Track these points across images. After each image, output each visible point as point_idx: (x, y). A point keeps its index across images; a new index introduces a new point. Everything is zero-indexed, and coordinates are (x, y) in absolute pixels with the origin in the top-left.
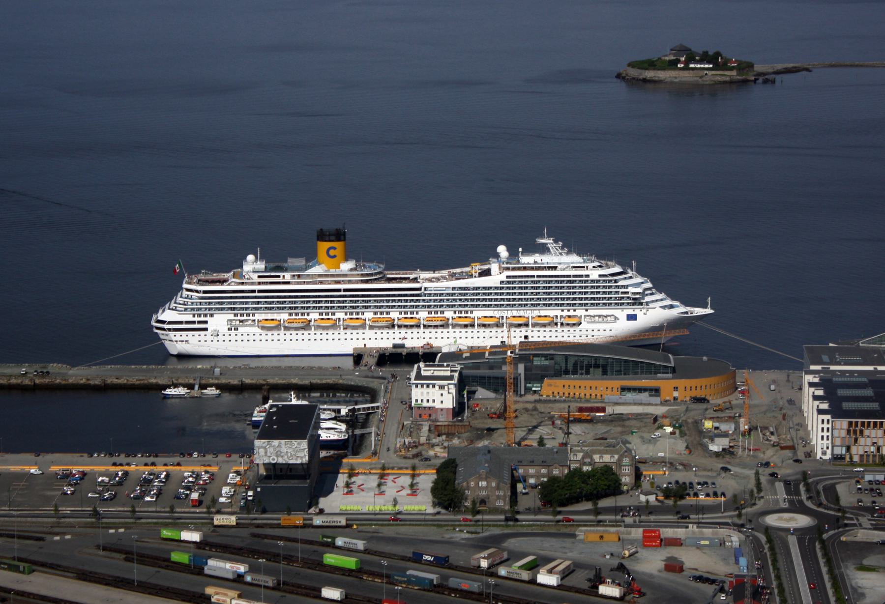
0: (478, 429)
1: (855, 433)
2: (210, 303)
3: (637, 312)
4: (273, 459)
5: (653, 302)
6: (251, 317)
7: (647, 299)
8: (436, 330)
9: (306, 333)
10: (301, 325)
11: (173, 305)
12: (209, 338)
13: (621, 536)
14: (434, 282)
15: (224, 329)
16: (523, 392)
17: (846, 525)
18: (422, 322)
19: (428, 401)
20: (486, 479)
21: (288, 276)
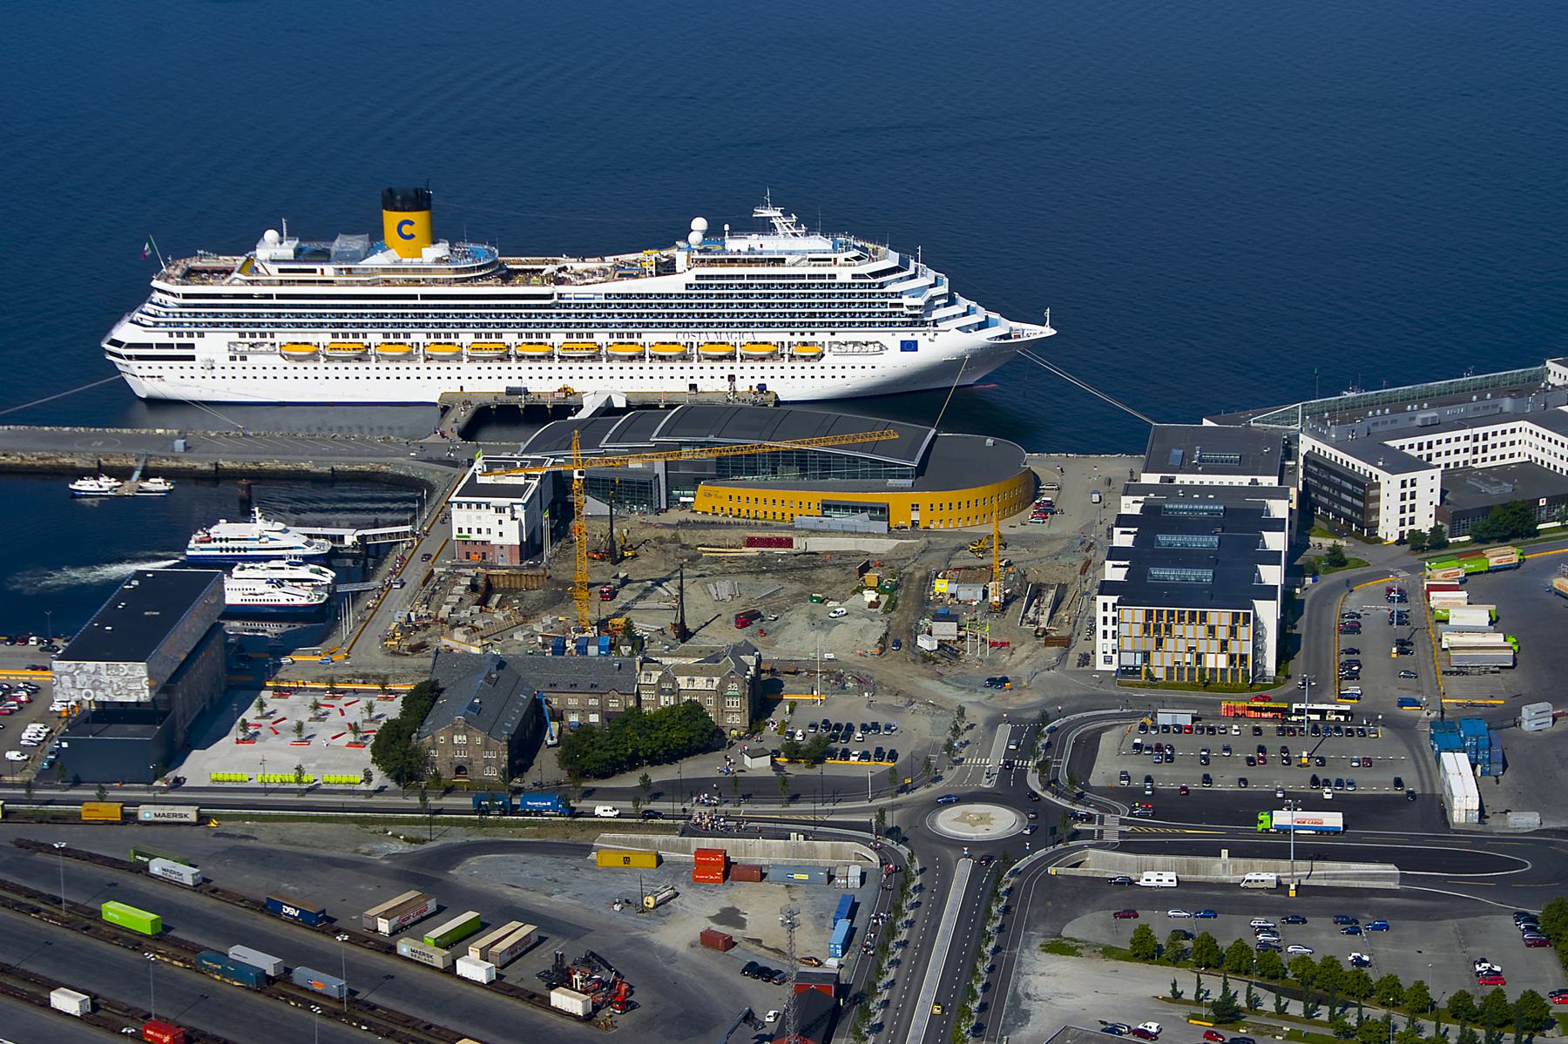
0: (559, 583)
1: (1157, 631)
2: (197, 315)
3: (918, 337)
4: (88, 694)
5: (947, 318)
6: (268, 339)
7: (936, 314)
8: (580, 364)
9: (362, 366)
10: (351, 353)
11: (137, 316)
12: (198, 372)
13: (665, 855)
14: (589, 280)
15: (222, 358)
16: (664, 506)
17: (1076, 835)
18: (556, 351)
19: (479, 531)
20: (465, 732)
21: (329, 271)
